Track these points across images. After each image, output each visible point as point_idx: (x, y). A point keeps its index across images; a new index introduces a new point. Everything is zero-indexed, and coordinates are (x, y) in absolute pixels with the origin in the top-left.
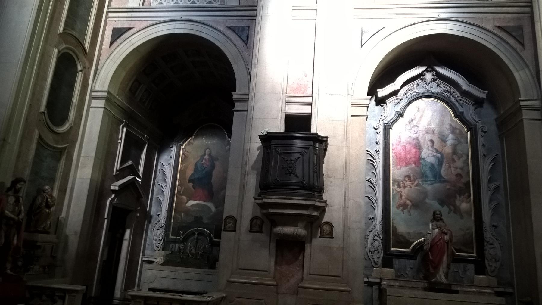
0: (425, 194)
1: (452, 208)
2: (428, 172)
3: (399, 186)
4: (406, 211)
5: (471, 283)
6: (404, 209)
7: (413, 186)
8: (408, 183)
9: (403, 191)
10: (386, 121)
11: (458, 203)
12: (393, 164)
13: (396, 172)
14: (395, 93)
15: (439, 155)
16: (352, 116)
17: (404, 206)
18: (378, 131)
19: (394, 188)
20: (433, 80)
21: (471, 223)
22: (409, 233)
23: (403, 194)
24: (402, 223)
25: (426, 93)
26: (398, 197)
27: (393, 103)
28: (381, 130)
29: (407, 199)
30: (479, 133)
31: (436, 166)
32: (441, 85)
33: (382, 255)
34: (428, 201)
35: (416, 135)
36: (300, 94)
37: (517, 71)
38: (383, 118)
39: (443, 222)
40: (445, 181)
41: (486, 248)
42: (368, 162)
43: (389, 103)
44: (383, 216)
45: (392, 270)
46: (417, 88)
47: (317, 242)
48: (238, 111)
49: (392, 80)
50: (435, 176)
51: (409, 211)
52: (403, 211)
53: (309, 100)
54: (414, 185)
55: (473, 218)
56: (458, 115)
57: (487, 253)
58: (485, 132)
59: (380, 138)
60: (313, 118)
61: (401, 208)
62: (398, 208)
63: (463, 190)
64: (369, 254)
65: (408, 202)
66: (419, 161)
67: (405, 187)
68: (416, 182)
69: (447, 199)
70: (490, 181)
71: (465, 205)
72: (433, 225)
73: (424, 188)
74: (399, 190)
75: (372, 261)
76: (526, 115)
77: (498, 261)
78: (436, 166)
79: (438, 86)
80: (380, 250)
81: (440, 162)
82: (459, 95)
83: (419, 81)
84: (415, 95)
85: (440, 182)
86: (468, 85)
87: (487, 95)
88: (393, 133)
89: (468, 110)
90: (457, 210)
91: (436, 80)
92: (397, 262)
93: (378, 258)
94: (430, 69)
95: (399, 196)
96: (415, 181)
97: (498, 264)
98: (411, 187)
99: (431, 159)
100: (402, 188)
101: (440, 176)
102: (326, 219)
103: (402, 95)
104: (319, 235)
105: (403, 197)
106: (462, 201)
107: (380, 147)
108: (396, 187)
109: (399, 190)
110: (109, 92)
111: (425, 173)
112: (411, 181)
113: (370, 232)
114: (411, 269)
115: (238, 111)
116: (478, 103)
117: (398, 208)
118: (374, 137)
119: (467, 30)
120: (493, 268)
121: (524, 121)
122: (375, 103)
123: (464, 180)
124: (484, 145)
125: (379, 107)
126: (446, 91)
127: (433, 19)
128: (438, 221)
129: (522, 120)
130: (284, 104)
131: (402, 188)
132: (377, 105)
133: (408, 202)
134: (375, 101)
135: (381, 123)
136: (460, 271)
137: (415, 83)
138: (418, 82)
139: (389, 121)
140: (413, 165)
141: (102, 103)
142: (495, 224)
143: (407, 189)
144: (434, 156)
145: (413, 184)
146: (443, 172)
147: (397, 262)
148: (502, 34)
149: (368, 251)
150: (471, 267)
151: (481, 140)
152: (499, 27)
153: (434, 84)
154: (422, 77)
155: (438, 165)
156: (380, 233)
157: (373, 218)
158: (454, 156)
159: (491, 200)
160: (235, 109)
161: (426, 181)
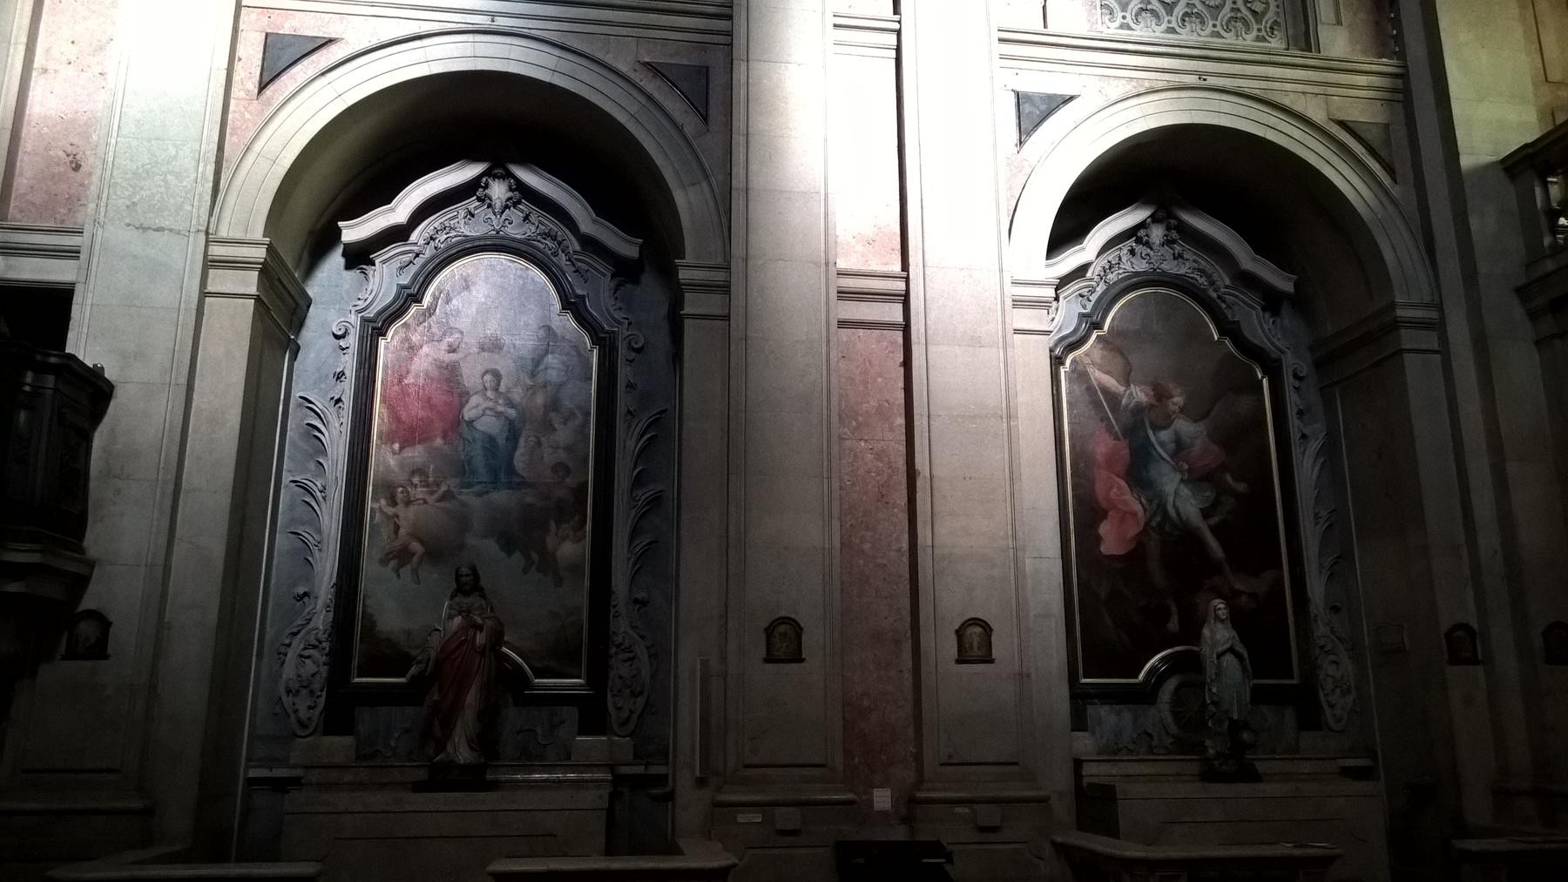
0: (462, 521)
1: (535, 557)
2: (480, 462)
3: (393, 502)
4: (406, 571)
5: (566, 758)
6: (401, 565)
7: (431, 499)
8: (420, 493)
9: (401, 515)
10: (370, 313)
11: (550, 541)
12: (380, 437)
13: (384, 458)
14: (397, 234)
15: (512, 412)
16: (1017, 331)
17: (401, 556)
18: (342, 343)
19: (376, 506)
20: (1169, 242)
21: (579, 597)
22: (409, 633)
23: (402, 523)
24: (393, 604)
25: (492, 237)
26: (386, 532)
27: (396, 264)
28: (352, 341)
29: (414, 535)
30: (622, 352)
31: (501, 441)
32: (533, 218)
33: (323, 699)
34: (471, 540)
35: (453, 357)
36: (51, 224)
37: (683, 187)
38: (362, 304)
39: (484, 596)
40: (523, 484)
41: (613, 661)
42: (309, 433)
43: (384, 262)
44: (339, 586)
45: (348, 740)
46: (460, 223)
47: (57, 672)
48: (1410, 351)
49: (386, 195)
50: (494, 473)
51: (415, 571)
52: (397, 571)
53: (719, 276)
54: (436, 496)
55: (587, 583)
56: (570, 303)
57: (612, 674)
58: (638, 351)
59: (349, 363)
60: (77, 299)
61: (393, 563)
62: (384, 562)
63: (566, 510)
64: (284, 698)
65: (416, 547)
66: (455, 424)
67: (408, 503)
68: (444, 488)
69: (522, 534)
70: (638, 482)
71: (571, 549)
72: (450, 607)
73: (464, 504)
74: (390, 511)
75: (293, 717)
76: (1408, 339)
77: (641, 693)
78: (501, 441)
79: (526, 218)
80: (316, 686)
81: (513, 433)
82: (578, 248)
83: (472, 204)
84: (460, 243)
85: (510, 486)
86: (595, 222)
87: (641, 247)
88: (387, 347)
89: (600, 291)
90: (546, 563)
91: (519, 202)
92: (366, 719)
93: (310, 708)
94: (499, 171)
95: (392, 527)
96: (438, 486)
97: (641, 701)
98: (425, 502)
99: (489, 425)
100: (401, 506)
101: (511, 470)
102: (88, 603)
103: (421, 242)
104: (62, 649)
105: (402, 531)
106: (564, 539)
107: (347, 389)
108: (383, 502)
109: (390, 511)
110: (271, 249)
111: (469, 462)
112: (427, 486)
113: (295, 634)
114: (407, 731)
115: (1410, 351)
116: (625, 271)
117: (384, 562)
118: (331, 361)
119: (565, 66)
120: (625, 715)
121: (1406, 356)
122: (342, 261)
123: (570, 481)
124: (630, 386)
125: (354, 274)
126: (547, 235)
127: (470, 27)
128: (467, 594)
129: (1401, 351)
130: (833, 295)
131: (401, 506)
132: (348, 267)
133: (416, 547)
134: (344, 255)
135: (354, 319)
136: (539, 730)
137: (460, 209)
138: (471, 207)
139: (380, 313)
140: (439, 441)
141: (249, 282)
142: (639, 596)
143: (412, 508)
144: (498, 415)
145: (432, 493)
146: (520, 460)
147: (366, 719)
148: (651, 86)
149: (282, 690)
150: (571, 714)
151: (624, 373)
152: (650, 67)
153: (515, 215)
154: (480, 192)
155: (507, 439)
156: (323, 637)
157: (306, 594)
158: (552, 414)
159: (635, 533)
160: (687, 310)
161: (469, 486)
